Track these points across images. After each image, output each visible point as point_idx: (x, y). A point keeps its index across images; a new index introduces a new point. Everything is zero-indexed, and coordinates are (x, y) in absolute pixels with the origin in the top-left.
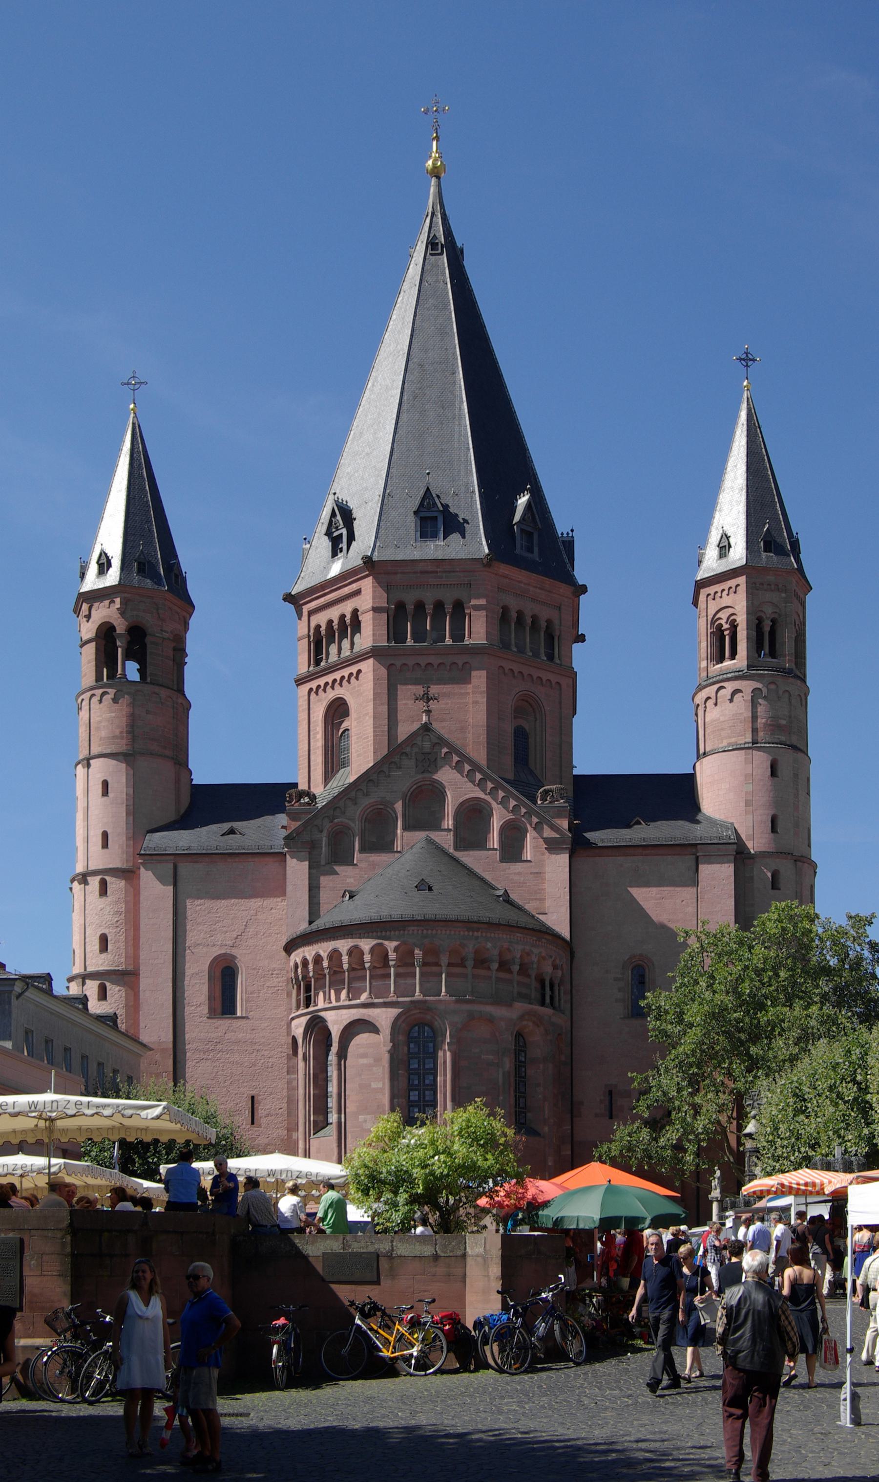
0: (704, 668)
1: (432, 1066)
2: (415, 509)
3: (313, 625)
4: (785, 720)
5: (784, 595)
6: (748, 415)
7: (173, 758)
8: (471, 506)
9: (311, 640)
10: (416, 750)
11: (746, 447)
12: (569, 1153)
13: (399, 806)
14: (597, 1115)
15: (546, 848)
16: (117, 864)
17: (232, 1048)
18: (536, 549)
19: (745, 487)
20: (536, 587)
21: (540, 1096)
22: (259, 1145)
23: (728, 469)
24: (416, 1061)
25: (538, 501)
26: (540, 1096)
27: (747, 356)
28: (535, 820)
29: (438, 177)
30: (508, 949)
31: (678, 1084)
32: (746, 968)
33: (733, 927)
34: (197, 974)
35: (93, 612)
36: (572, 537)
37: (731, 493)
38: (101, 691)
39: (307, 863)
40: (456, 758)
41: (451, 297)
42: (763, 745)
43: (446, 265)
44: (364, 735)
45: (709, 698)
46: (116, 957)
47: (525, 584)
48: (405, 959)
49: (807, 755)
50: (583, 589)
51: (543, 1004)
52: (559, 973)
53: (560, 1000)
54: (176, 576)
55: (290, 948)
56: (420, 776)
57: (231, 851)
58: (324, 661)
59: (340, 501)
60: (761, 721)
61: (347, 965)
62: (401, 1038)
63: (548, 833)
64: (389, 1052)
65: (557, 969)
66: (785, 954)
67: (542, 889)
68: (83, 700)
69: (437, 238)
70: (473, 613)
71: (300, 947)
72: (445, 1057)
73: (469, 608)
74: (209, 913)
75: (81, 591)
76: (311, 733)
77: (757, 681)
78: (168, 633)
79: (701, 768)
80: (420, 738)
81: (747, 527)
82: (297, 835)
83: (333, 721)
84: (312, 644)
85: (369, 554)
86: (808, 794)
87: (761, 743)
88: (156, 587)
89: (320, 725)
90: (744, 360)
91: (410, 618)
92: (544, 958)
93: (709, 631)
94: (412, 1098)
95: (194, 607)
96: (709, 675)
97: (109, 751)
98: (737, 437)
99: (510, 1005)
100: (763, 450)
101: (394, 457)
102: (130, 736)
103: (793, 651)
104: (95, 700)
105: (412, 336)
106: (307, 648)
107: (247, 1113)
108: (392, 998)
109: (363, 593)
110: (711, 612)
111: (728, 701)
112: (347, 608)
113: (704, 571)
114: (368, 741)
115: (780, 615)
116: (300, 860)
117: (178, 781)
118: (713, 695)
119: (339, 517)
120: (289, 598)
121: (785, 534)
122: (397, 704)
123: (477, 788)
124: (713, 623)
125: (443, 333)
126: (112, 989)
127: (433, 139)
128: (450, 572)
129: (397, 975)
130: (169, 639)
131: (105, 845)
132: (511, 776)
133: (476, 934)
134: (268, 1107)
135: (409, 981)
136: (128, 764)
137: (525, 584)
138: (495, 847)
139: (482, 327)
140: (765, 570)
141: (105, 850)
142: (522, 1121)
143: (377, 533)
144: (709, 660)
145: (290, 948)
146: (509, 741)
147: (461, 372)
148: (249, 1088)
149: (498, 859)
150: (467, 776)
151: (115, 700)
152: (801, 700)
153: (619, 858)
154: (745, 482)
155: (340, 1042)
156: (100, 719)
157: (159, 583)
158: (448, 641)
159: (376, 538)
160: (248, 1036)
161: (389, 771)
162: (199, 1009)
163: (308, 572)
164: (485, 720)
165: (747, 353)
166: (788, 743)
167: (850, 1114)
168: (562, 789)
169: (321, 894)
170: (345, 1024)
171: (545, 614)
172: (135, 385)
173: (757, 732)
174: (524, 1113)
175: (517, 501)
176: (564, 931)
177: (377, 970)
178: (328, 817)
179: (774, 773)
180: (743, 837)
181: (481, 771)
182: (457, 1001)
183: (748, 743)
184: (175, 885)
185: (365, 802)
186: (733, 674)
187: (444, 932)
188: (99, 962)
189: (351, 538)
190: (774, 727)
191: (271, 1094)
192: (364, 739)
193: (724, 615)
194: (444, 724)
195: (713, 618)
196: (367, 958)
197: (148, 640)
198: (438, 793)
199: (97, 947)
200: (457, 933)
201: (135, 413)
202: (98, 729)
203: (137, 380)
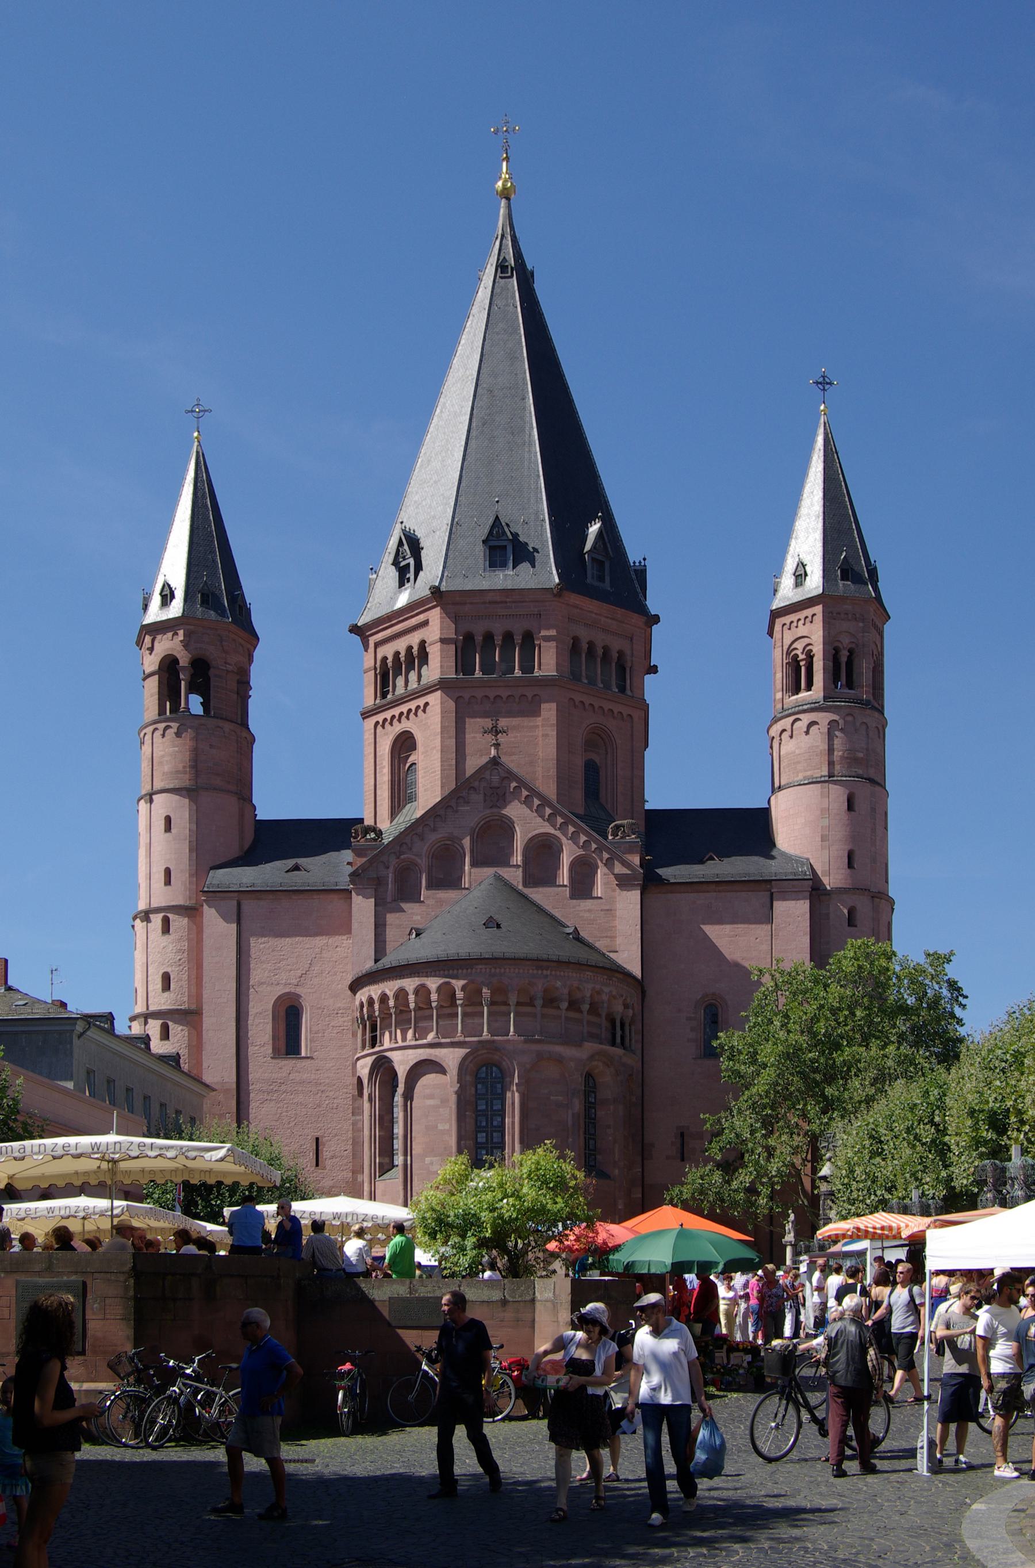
2: (484, 538)
5: (861, 624)
9: (378, 671)
13: (467, 842)
16: (180, 901)
18: (607, 579)
19: (821, 514)
20: (607, 617)
23: (805, 495)
25: (610, 530)
28: (606, 855)
29: (508, 199)
30: (578, 988)
31: (752, 1125)
32: (822, 1007)
33: (808, 965)
35: (156, 644)
36: (645, 566)
37: (808, 520)
38: (163, 725)
39: (373, 900)
40: (525, 793)
42: (839, 778)
43: (516, 288)
45: (784, 730)
47: (596, 614)
48: (473, 999)
50: (656, 619)
51: (613, 1044)
52: (630, 1012)
55: (355, 986)
56: (488, 811)
58: (391, 693)
59: (407, 530)
60: (837, 754)
62: (468, 1078)
63: (619, 869)
64: (456, 1093)
65: (628, 1008)
68: (145, 734)
70: (543, 644)
71: (366, 986)
72: (514, 1098)
74: (273, 951)
75: (144, 623)
79: (776, 802)
80: (488, 772)
81: (824, 555)
83: (399, 755)
85: (437, 584)
88: (220, 618)
89: (387, 759)
91: (478, 649)
92: (614, 997)
94: (479, 1140)
95: (253, 637)
97: (171, 786)
99: (579, 1045)
100: (841, 476)
101: (463, 484)
104: (158, 734)
105: (481, 361)
107: (312, 1155)
108: (459, 1037)
109: (430, 624)
110: (787, 642)
112: (414, 640)
115: (857, 645)
117: (242, 815)
118: (788, 727)
119: (406, 547)
120: (355, 629)
121: (863, 562)
123: (546, 823)
124: (788, 653)
125: (513, 358)
127: (503, 160)
129: (465, 1015)
130: (233, 671)
131: (168, 881)
132: (581, 811)
133: (545, 972)
135: (477, 1020)
136: (191, 799)
137: (596, 614)
138: (565, 883)
139: (553, 350)
142: (592, 1163)
143: (445, 562)
145: (355, 986)
150: (536, 811)
151: (178, 734)
153: (692, 895)
154: (821, 509)
158: (517, 672)
159: (444, 567)
160: (313, 1076)
162: (262, 1049)
165: (824, 377)
166: (865, 776)
167: (927, 1156)
168: (633, 824)
169: (387, 932)
171: (616, 645)
172: (199, 413)
174: (593, 1155)
175: (588, 529)
176: (635, 968)
178: (394, 853)
179: (850, 807)
180: (819, 873)
181: (551, 805)
182: (526, 1041)
185: (432, 837)
186: (808, 706)
188: (161, 1001)
189: (419, 567)
190: (852, 760)
191: (336, 1135)
192: (432, 773)
193: (800, 645)
194: (514, 757)
196: (434, 997)
197: (212, 672)
198: (507, 828)
201: (199, 442)
202: (161, 763)
203: (202, 408)
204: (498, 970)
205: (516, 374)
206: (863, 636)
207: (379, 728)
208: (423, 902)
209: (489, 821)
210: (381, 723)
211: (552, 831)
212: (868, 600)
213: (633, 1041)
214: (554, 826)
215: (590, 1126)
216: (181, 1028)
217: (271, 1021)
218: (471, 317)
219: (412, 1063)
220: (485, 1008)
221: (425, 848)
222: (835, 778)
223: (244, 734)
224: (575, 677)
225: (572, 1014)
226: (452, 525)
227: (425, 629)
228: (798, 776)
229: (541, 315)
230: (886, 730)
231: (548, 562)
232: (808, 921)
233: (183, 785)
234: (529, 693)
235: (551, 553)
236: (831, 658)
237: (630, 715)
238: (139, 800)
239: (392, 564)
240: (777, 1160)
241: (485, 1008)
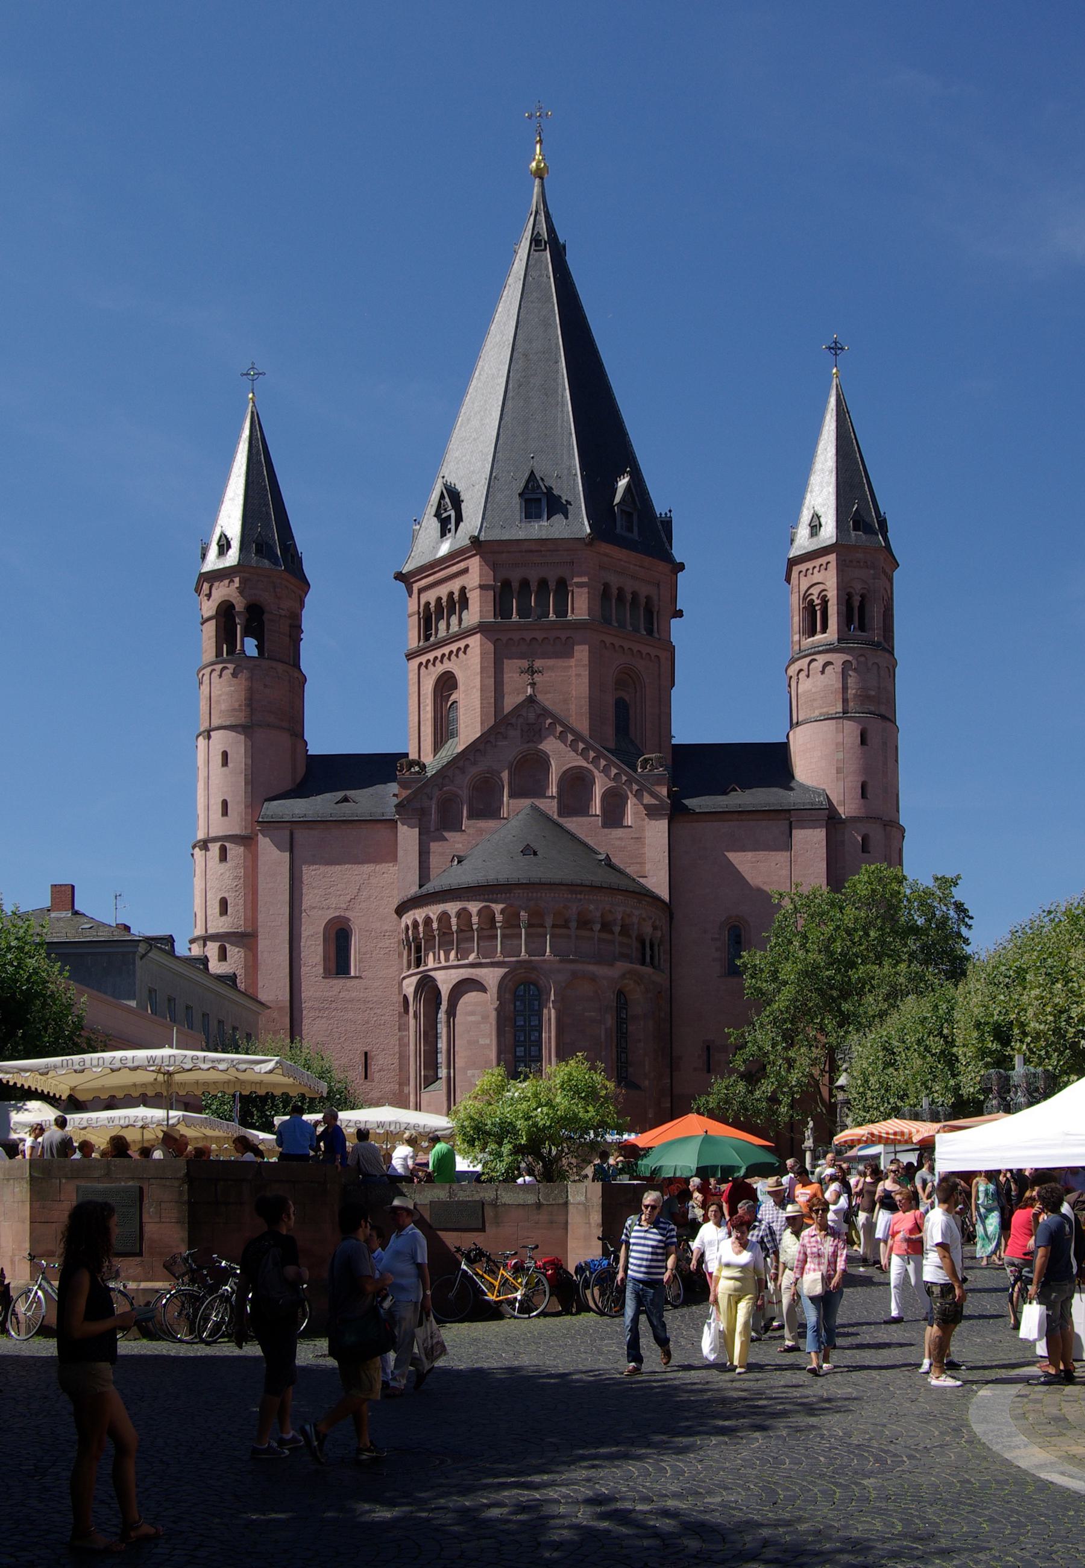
1: (537, 1023)
3: (422, 602)
5: (872, 572)
8: (574, 488)
12: (669, 1105)
13: (505, 775)
16: (236, 831)
18: (635, 529)
20: (636, 565)
23: (819, 452)
25: (638, 482)
28: (635, 787)
29: (541, 178)
30: (610, 911)
31: (773, 1039)
32: (838, 927)
36: (670, 517)
38: (221, 666)
39: (417, 829)
40: (559, 729)
45: (801, 670)
47: (625, 562)
48: (512, 921)
50: (681, 567)
52: (659, 934)
53: (659, 959)
55: (401, 910)
58: (433, 636)
60: (851, 692)
62: (507, 996)
63: (648, 799)
64: (496, 1009)
70: (576, 590)
72: (550, 1014)
74: (324, 877)
75: (202, 571)
79: (795, 737)
83: (442, 693)
85: (476, 534)
86: (897, 761)
91: (515, 595)
92: (644, 919)
93: (801, 606)
94: (518, 1054)
95: (304, 584)
97: (228, 723)
99: (612, 965)
101: (500, 442)
103: (881, 625)
104: (215, 675)
105: (517, 327)
108: (499, 957)
109: (470, 571)
110: (803, 588)
112: (455, 586)
116: (412, 827)
118: (805, 667)
119: (447, 500)
120: (400, 577)
121: (873, 514)
123: (580, 757)
124: (805, 598)
125: (547, 324)
127: (537, 142)
129: (503, 936)
130: (285, 616)
131: (225, 813)
132: (611, 745)
133: (579, 896)
135: (515, 942)
136: (246, 736)
137: (625, 562)
138: (598, 813)
142: (624, 1075)
143: (484, 514)
145: (401, 910)
150: (570, 746)
151: (234, 675)
156: (220, 692)
157: (276, 563)
158: (552, 616)
159: (483, 519)
160: (362, 995)
165: (836, 343)
171: (644, 590)
172: (253, 375)
176: (665, 894)
179: (863, 741)
180: (835, 803)
182: (561, 961)
185: (473, 771)
186: (824, 647)
188: (219, 925)
189: (459, 519)
190: (864, 697)
193: (815, 591)
194: (549, 696)
197: (266, 617)
198: (542, 762)
199: (217, 910)
201: (253, 402)
202: (218, 702)
203: (256, 371)
205: (550, 340)
208: (464, 831)
209: (526, 755)
211: (585, 764)
214: (587, 759)
216: (237, 949)
219: (454, 982)
222: (849, 715)
224: (606, 620)
225: (605, 936)
229: (572, 284)
233: (238, 722)
236: (845, 604)
238: (198, 737)
239: (435, 516)
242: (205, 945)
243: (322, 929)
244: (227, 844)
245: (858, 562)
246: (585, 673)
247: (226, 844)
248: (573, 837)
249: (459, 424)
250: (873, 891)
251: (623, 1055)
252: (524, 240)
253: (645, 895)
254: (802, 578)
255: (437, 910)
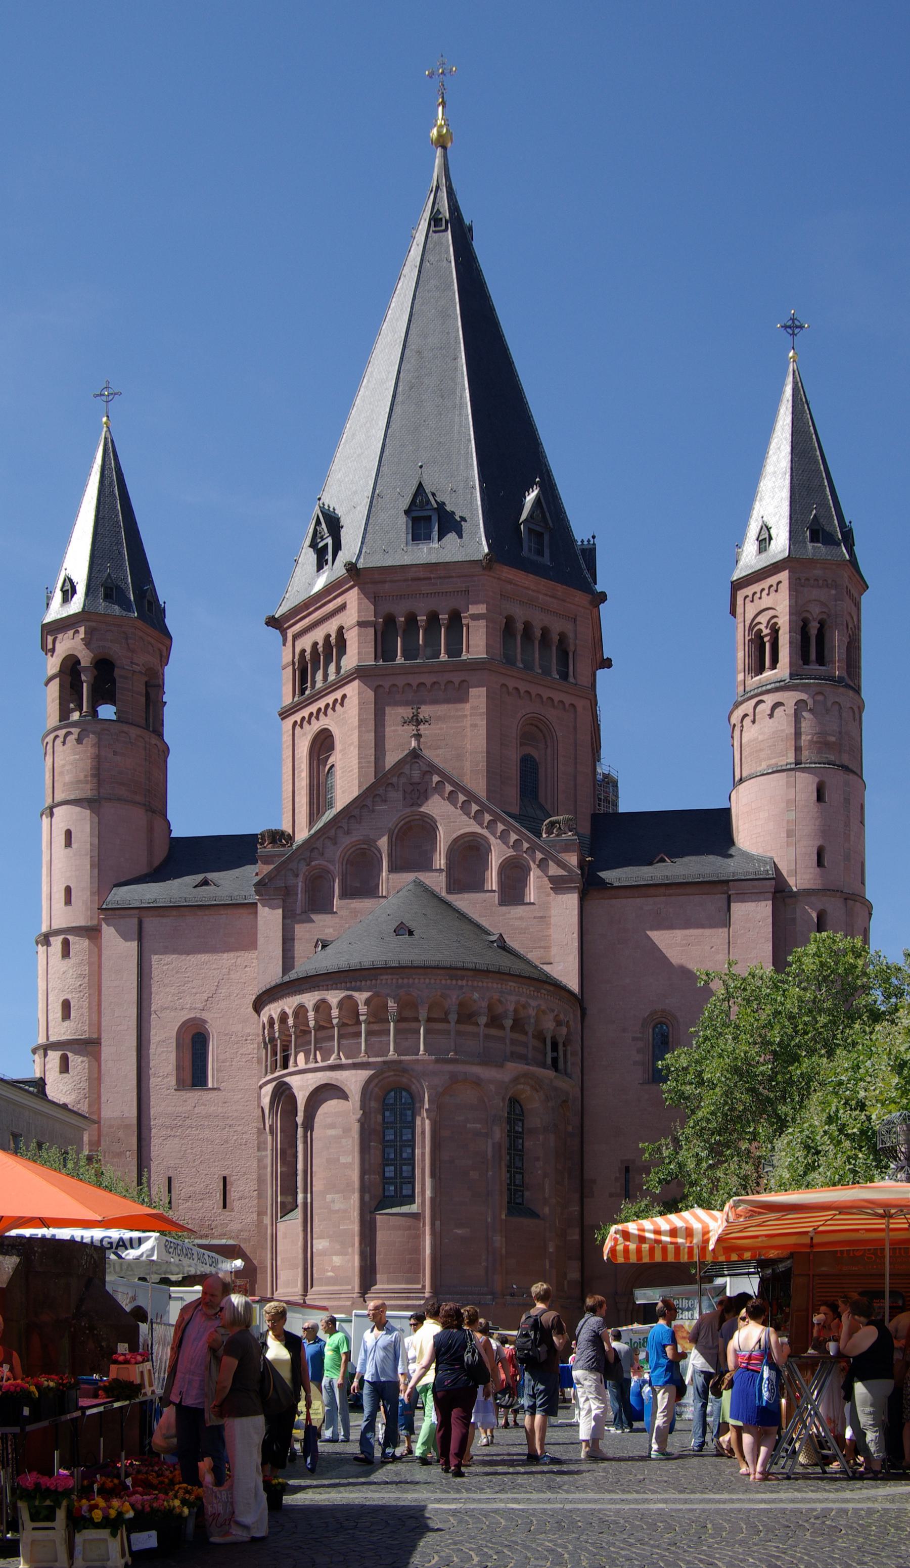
0: (741, 681)
1: (410, 1136)
2: (406, 507)
3: (298, 650)
4: (834, 736)
5: (833, 592)
6: (793, 389)
7: (145, 805)
8: (471, 503)
9: (296, 667)
10: (403, 780)
11: (791, 425)
12: (577, 1237)
13: (383, 843)
14: (611, 1195)
15: (551, 888)
16: (81, 922)
17: (202, 1123)
18: (547, 552)
19: (789, 470)
20: (546, 595)
21: (539, 1172)
22: (231, 1231)
23: (771, 452)
24: (392, 1131)
25: (550, 494)
26: (539, 1172)
27: (793, 322)
28: (539, 856)
29: (444, 148)
30: (500, 1001)
31: (697, 1154)
32: (777, 1013)
33: (769, 969)
34: (163, 1041)
35: (58, 645)
36: (594, 544)
37: (774, 479)
38: (64, 731)
39: (280, 911)
40: (449, 788)
41: (455, 276)
42: (807, 766)
43: (451, 241)
44: (349, 767)
45: (746, 715)
46: (80, 1025)
47: (533, 591)
48: (378, 1015)
49: (862, 779)
50: (603, 597)
51: (543, 1065)
52: (564, 1030)
53: (565, 1062)
54: (150, 603)
55: (258, 1005)
56: (408, 810)
57: (201, 903)
58: (309, 689)
59: (326, 507)
60: (805, 739)
61: (314, 1022)
62: (373, 1104)
63: (554, 870)
64: (359, 1121)
65: (561, 1025)
66: (824, 995)
67: (547, 936)
68: (47, 743)
69: (440, 213)
70: (472, 624)
71: (267, 1005)
72: (424, 1125)
73: (466, 617)
74: (177, 972)
75: (45, 622)
76: (296, 772)
77: (802, 691)
78: (138, 665)
79: (737, 797)
80: (408, 766)
81: (790, 515)
82: (269, 880)
83: (318, 757)
84: (297, 672)
85: (354, 561)
86: (862, 823)
87: (805, 763)
88: (124, 613)
89: (305, 762)
90: (790, 327)
91: (400, 632)
92: (544, 1012)
93: (747, 638)
94: (387, 1174)
95: (171, 638)
96: (746, 690)
97: (72, 797)
98: (780, 415)
99: (501, 1066)
100: (812, 428)
101: (386, 453)
102: (95, 780)
103: (844, 656)
104: (59, 741)
105: (410, 321)
106: (291, 677)
107: (219, 1196)
108: (362, 1058)
109: (348, 607)
110: (749, 616)
111: (768, 717)
112: (331, 627)
113: (742, 569)
114: (353, 775)
115: (829, 616)
116: (272, 907)
117: (151, 829)
118: (751, 712)
119: (324, 525)
120: (273, 622)
121: (836, 522)
122: (385, 732)
123: (472, 821)
124: (751, 628)
125: (445, 315)
126: (76, 1060)
127: (439, 105)
128: (445, 578)
129: (369, 1033)
130: (140, 672)
131: (68, 901)
132: (516, 810)
133: (460, 982)
134: (241, 1189)
135: (384, 1038)
136: (92, 810)
137: (533, 591)
138: (494, 888)
139: (492, 309)
140: (812, 562)
141: (69, 907)
142: (519, 1201)
143: (364, 538)
144: (747, 673)
145: (258, 1005)
146: (514, 772)
147: (463, 357)
148: (220, 1167)
149: (497, 902)
150: (461, 808)
151: (79, 741)
152: (854, 712)
153: (638, 899)
154: (789, 465)
155: (306, 1111)
156: (63, 762)
157: (128, 609)
158: (443, 657)
159: (362, 543)
160: (220, 1110)
161: (373, 805)
162: (165, 1080)
163: (293, 591)
164: (485, 745)
165: (793, 320)
166: (837, 763)
167: (857, 1156)
168: (571, 820)
169: (296, 948)
170: (311, 1090)
171: (557, 626)
172: (108, 395)
173: (801, 751)
174: (520, 1191)
175: (525, 498)
176: (573, 983)
177: (350, 1028)
178: (304, 859)
179: (820, 798)
180: (785, 873)
181: (478, 801)
182: (437, 1061)
183: (791, 764)
184: (140, 940)
185: (346, 841)
186: (773, 685)
187: (422, 980)
188: (61, 1031)
189: (337, 547)
190: (822, 744)
191: (245, 1174)
192: (349, 772)
193: (763, 619)
194: (440, 752)
195: (750, 627)
196: (335, 1012)
197: (117, 672)
198: (428, 827)
199: (59, 1014)
200: (438, 981)
201: (108, 427)
202: (62, 773)
203: (111, 391)
204: (406, 981)
205: (448, 333)
206: (836, 605)
207: (298, 728)
208: (336, 913)
209: (410, 821)
210: (299, 723)
211: (479, 830)
212: (842, 563)
213: (569, 1063)
214: (481, 824)
215: (517, 1159)
216: (81, 1059)
217: (175, 1050)
218: (402, 279)
219: (311, 1089)
220: (392, 1023)
221: (338, 853)
222: (803, 766)
223: (154, 740)
224: (509, 661)
225: (493, 1032)
226: (372, 497)
227: (344, 612)
228: (761, 765)
229: (478, 272)
230: (864, 715)
231: (477, 533)
232: (771, 926)
233: (83, 796)
234: (456, 678)
235: (481, 522)
236: (799, 631)
237: (573, 705)
238: (41, 816)
239: (310, 546)
240: (721, 1192)
241: (392, 1023)
242: (45, 1055)
243: (174, 1033)
244: (70, 937)
245: (816, 580)
246: (482, 723)
247: (68, 937)
248: (462, 916)
249: (343, 440)
250: (822, 964)
251: (517, 1176)
252: (423, 220)
253: (545, 982)
254: (749, 605)
255: (293, 1003)
